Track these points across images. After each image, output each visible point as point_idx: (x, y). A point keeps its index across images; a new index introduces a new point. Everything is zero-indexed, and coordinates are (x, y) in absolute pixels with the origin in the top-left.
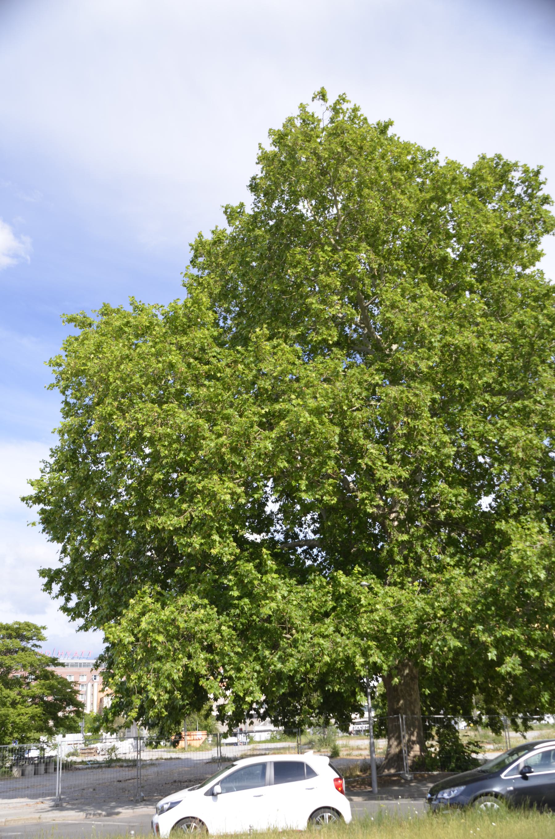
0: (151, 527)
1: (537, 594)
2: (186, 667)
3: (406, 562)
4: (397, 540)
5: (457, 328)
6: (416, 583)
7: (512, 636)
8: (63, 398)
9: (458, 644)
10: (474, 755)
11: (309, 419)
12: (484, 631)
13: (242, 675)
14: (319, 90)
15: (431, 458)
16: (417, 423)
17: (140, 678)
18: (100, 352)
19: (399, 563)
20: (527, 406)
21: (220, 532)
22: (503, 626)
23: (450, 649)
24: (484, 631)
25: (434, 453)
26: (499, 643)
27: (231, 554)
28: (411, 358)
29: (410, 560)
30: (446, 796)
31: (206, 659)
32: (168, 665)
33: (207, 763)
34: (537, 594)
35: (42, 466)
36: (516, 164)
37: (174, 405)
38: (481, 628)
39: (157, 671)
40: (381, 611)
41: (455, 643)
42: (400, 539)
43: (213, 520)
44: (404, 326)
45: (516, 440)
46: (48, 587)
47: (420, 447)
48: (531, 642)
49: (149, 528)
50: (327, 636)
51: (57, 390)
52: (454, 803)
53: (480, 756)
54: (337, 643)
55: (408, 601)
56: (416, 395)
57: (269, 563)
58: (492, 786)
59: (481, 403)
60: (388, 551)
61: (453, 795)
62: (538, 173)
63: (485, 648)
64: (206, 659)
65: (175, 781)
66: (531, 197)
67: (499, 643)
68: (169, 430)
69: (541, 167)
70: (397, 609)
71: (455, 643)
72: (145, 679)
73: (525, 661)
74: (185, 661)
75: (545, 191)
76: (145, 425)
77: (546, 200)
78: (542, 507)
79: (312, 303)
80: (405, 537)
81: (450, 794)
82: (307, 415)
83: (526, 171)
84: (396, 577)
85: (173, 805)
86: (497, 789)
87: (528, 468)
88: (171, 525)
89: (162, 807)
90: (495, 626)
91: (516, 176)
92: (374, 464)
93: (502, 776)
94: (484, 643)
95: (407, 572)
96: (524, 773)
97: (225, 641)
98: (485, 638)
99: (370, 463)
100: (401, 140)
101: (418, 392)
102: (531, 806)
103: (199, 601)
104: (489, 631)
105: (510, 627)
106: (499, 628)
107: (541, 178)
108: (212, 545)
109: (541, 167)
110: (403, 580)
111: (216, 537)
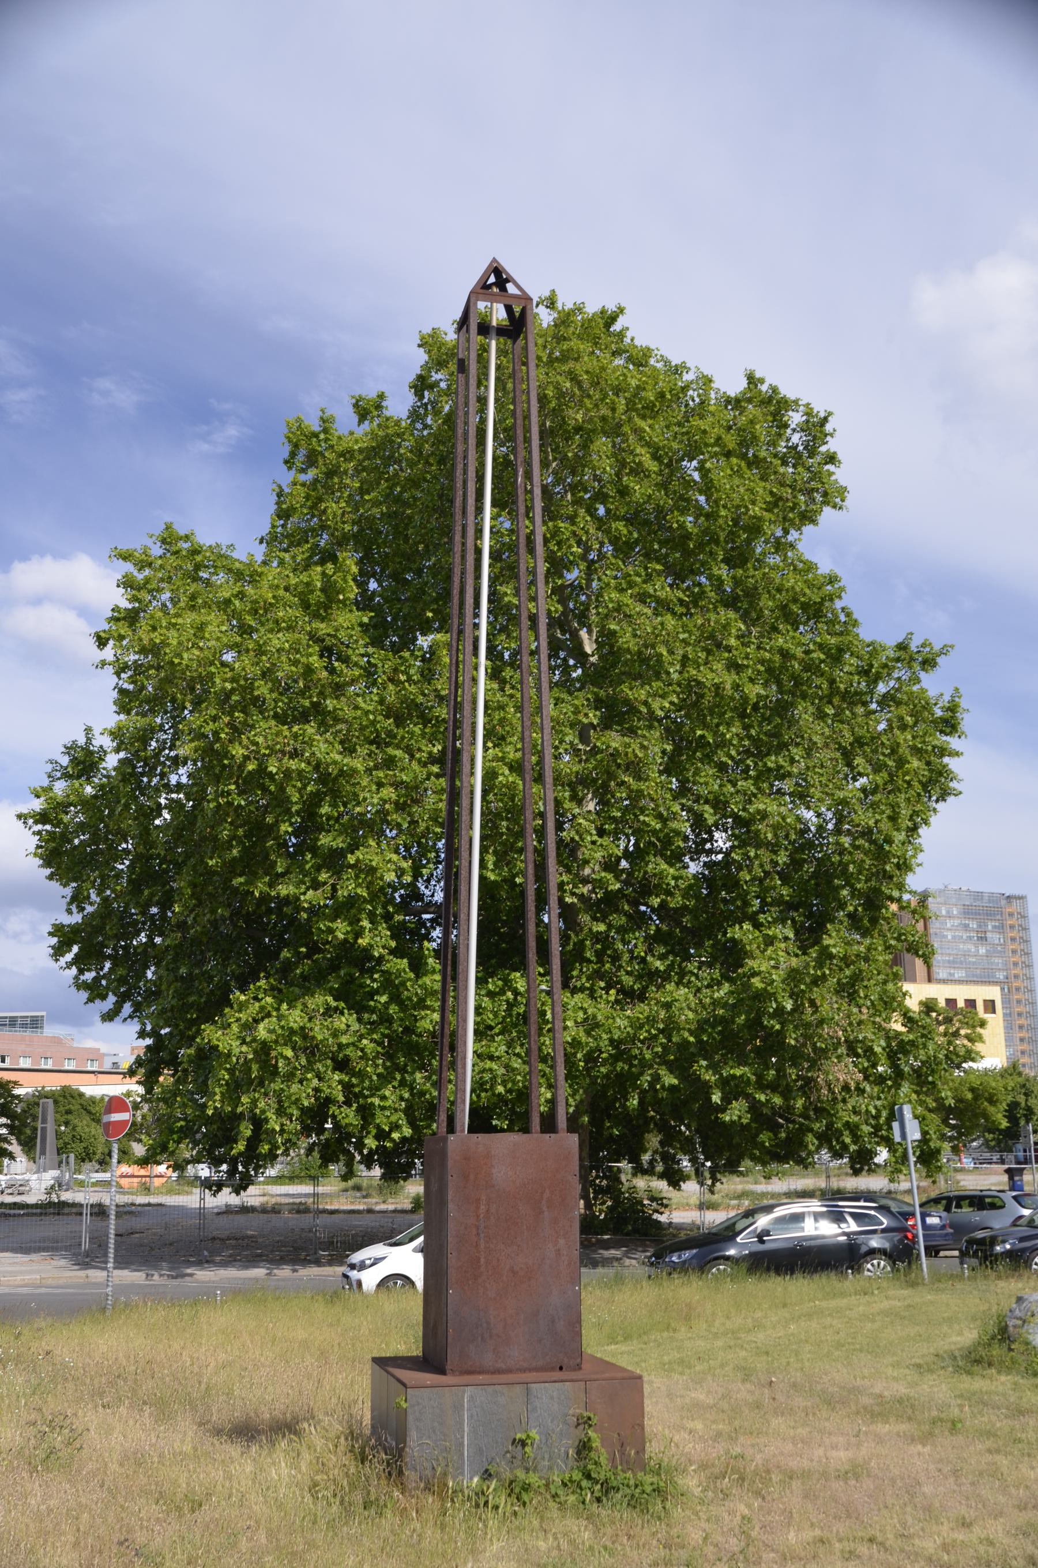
0: (261, 893)
1: (778, 1027)
2: (317, 1090)
3: (600, 961)
4: (590, 929)
5: (703, 655)
6: (613, 992)
7: (742, 1076)
8: (115, 679)
9: (675, 1082)
10: (656, 1216)
11: (511, 779)
12: (707, 1068)
13: (387, 1104)
14: (547, 294)
15: (654, 832)
16: (643, 786)
17: (254, 1102)
18: (202, 638)
19: (589, 961)
20: (782, 767)
21: (372, 918)
22: (731, 1063)
23: (663, 1087)
24: (707, 1068)
25: (658, 826)
26: (725, 1083)
27: (384, 947)
28: (642, 694)
29: (606, 958)
30: (674, 1259)
31: (340, 1082)
32: (295, 1087)
33: (218, 1214)
34: (778, 1027)
35: (49, 768)
36: (796, 402)
37: (310, 729)
38: (704, 1063)
39: (278, 1094)
40: (572, 1031)
41: (670, 1080)
42: (595, 929)
43: (365, 901)
44: (633, 645)
45: (764, 815)
46: (58, 952)
47: (642, 818)
48: (762, 1085)
49: (257, 894)
50: (499, 1058)
51: (110, 670)
52: (683, 1268)
53: (663, 1218)
54: (514, 1070)
55: (607, 1018)
56: (643, 747)
57: (431, 961)
58: (728, 1249)
59: (724, 759)
60: (575, 944)
61: (684, 1257)
62: (825, 420)
63: (706, 1089)
64: (340, 1082)
65: (214, 1239)
66: (812, 452)
67: (725, 1083)
68: (303, 765)
69: (830, 414)
70: (591, 1025)
71: (670, 1080)
72: (261, 1104)
73: (754, 1107)
74: (315, 1082)
75: (832, 445)
76: (269, 755)
77: (831, 459)
78: (787, 902)
79: (506, 594)
80: (602, 928)
81: (680, 1257)
82: (507, 772)
83: (809, 413)
84: (584, 980)
85: (376, 1261)
86: (732, 1252)
87: (775, 853)
88: (306, 901)
89: (363, 1262)
90: (720, 1061)
91: (795, 418)
92: (582, 839)
93: (738, 1239)
94: (707, 1083)
95: (598, 975)
96: (761, 1237)
97: (368, 1060)
98: (709, 1077)
99: (577, 838)
100: (637, 342)
101: (646, 743)
102: (768, 1270)
103: (334, 1004)
104: (714, 1067)
105: (740, 1064)
106: (726, 1064)
107: (828, 428)
108: (359, 933)
109: (830, 414)
110: (593, 985)
111: (366, 923)
